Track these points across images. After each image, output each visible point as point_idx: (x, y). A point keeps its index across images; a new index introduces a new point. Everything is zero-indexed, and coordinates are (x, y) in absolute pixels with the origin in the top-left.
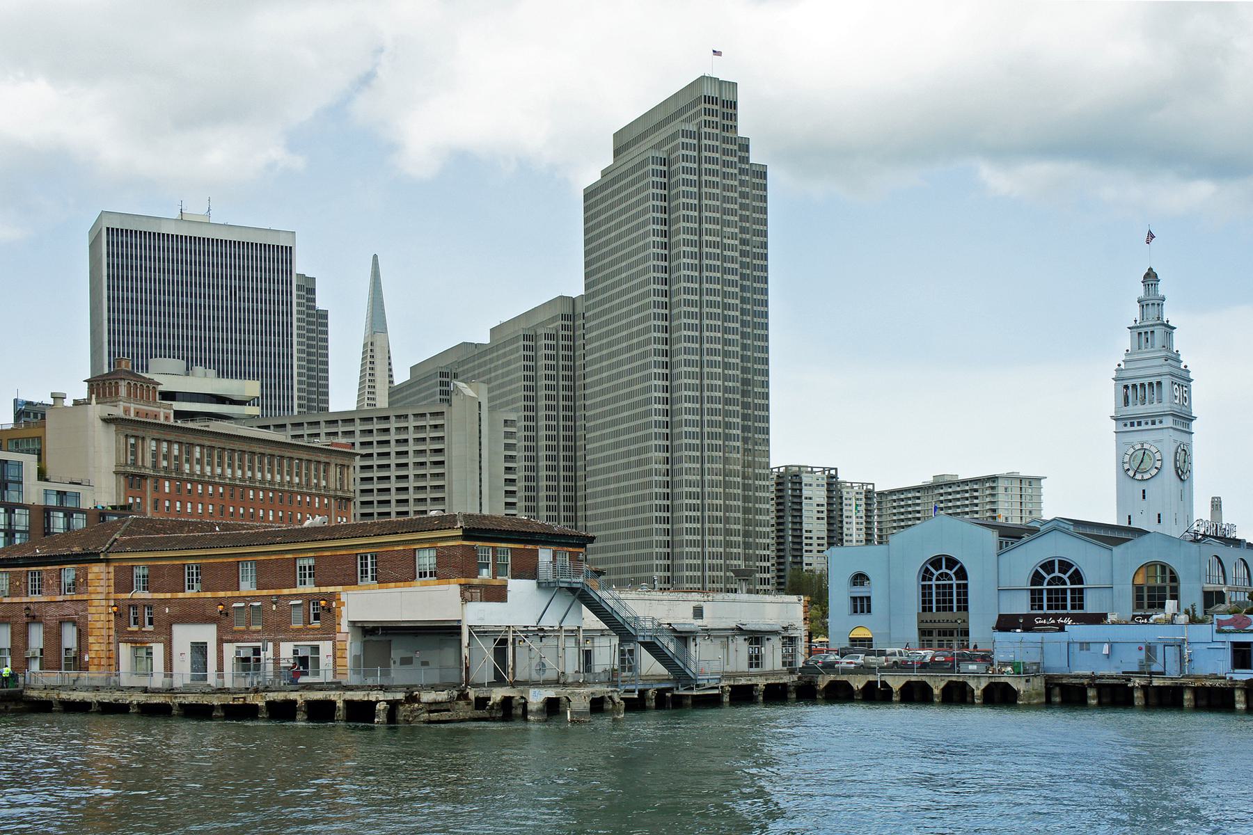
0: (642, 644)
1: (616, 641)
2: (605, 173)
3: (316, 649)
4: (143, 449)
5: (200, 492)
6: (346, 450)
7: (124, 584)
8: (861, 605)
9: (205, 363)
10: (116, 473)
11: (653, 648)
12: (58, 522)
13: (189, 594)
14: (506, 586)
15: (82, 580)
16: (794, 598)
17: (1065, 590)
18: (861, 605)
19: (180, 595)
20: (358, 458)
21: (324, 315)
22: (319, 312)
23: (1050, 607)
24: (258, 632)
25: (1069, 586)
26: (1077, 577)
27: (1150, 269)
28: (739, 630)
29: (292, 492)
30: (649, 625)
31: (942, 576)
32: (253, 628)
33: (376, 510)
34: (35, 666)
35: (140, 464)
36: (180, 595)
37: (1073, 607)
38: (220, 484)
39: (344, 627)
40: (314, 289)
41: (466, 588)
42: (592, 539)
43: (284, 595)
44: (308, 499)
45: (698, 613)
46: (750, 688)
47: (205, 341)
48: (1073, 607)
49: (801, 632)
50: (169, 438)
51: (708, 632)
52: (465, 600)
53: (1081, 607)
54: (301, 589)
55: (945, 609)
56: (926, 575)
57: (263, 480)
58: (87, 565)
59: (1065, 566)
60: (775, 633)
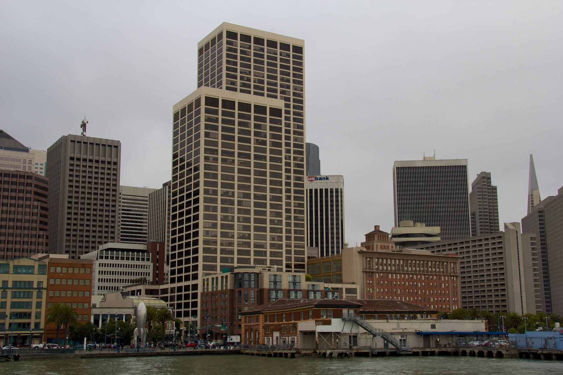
4: (372, 262)
5: (403, 277)
6: (454, 256)
9: (421, 222)
10: (363, 272)
12: (312, 295)
14: (331, 321)
19: (274, 323)
20: (459, 259)
21: (495, 188)
22: (493, 187)
29: (440, 275)
35: (371, 268)
36: (274, 323)
38: (402, 274)
39: (298, 333)
40: (490, 178)
41: (316, 321)
44: (431, 277)
45: (433, 326)
46: (434, 352)
47: (434, 208)
50: (382, 257)
52: (316, 325)
57: (420, 271)
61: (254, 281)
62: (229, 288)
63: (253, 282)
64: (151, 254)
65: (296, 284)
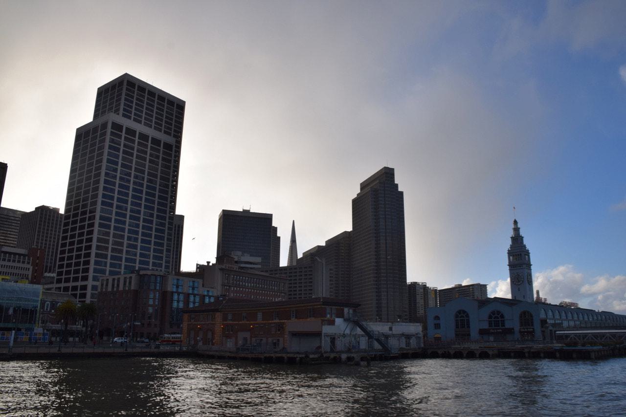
0: (375, 339)
1: (367, 338)
2: (358, 195)
3: (278, 340)
7: (225, 318)
8: (437, 326)
11: (378, 340)
13: (243, 322)
16: (419, 324)
17: (499, 321)
18: (437, 326)
19: (240, 322)
23: (495, 326)
24: (262, 334)
25: (500, 319)
26: (502, 316)
28: (403, 335)
30: (377, 333)
31: (461, 317)
32: (261, 333)
33: (293, 297)
34: (200, 344)
37: (502, 326)
41: (323, 321)
42: (360, 305)
45: (391, 329)
46: (407, 354)
48: (502, 326)
49: (421, 335)
51: (394, 336)
53: (504, 326)
54: (275, 321)
55: (463, 327)
56: (457, 316)
59: (499, 312)
60: (414, 335)
61: (150, 282)
62: (133, 288)
63: (158, 285)
64: (31, 258)
65: (178, 287)
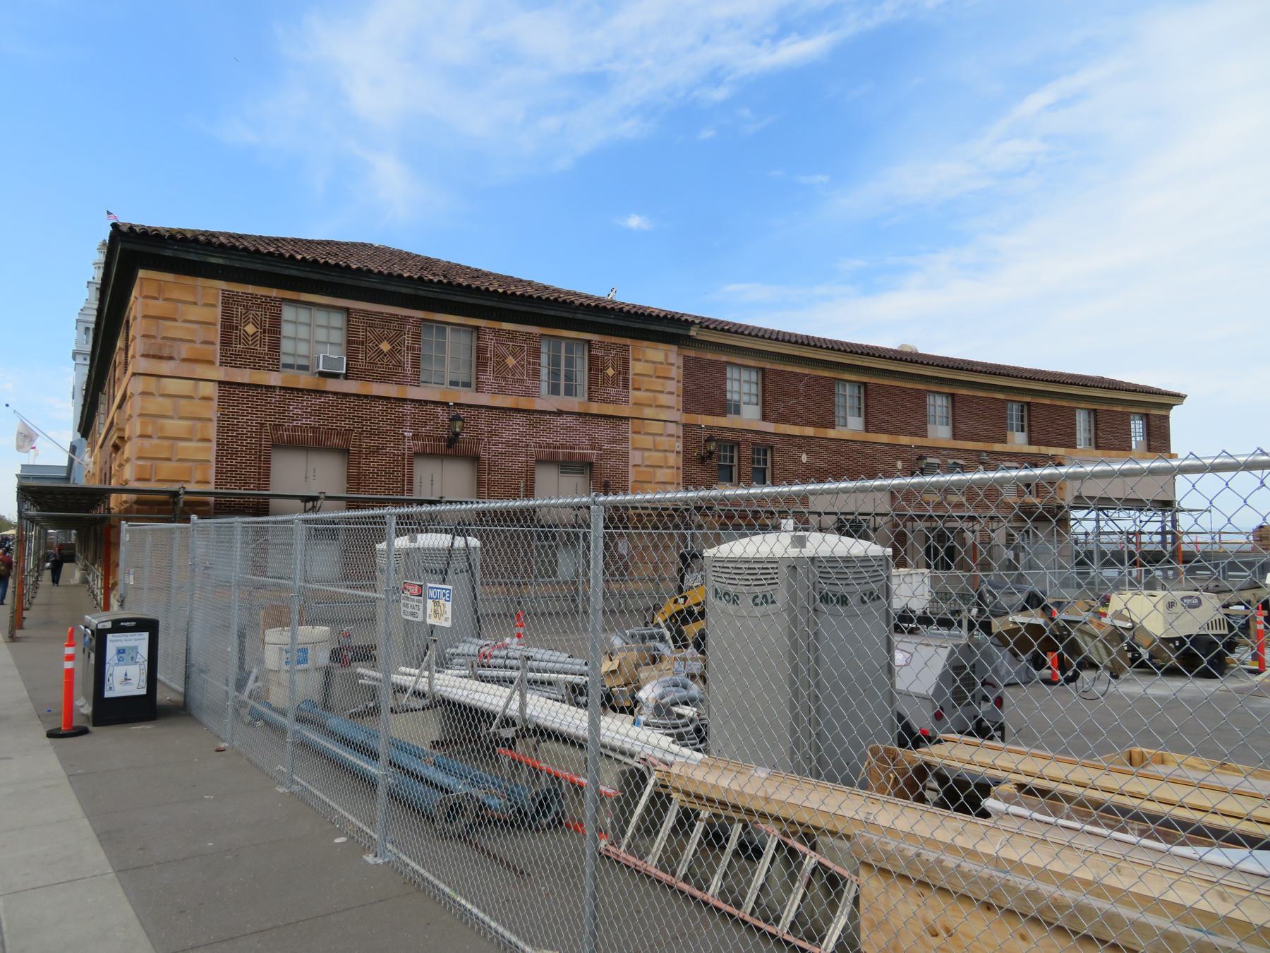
14: (990, 622)
15: (610, 372)
27: (1180, 397)
43: (902, 446)
58: (628, 341)
